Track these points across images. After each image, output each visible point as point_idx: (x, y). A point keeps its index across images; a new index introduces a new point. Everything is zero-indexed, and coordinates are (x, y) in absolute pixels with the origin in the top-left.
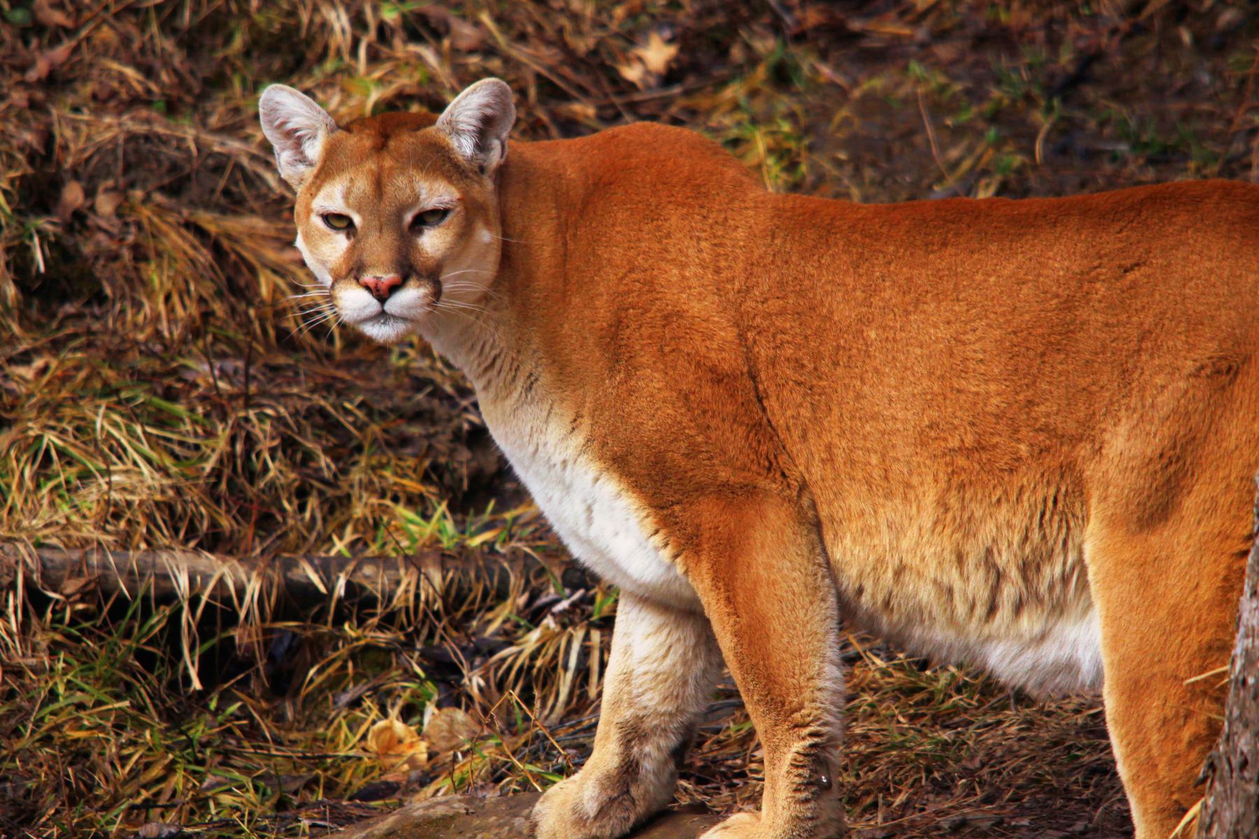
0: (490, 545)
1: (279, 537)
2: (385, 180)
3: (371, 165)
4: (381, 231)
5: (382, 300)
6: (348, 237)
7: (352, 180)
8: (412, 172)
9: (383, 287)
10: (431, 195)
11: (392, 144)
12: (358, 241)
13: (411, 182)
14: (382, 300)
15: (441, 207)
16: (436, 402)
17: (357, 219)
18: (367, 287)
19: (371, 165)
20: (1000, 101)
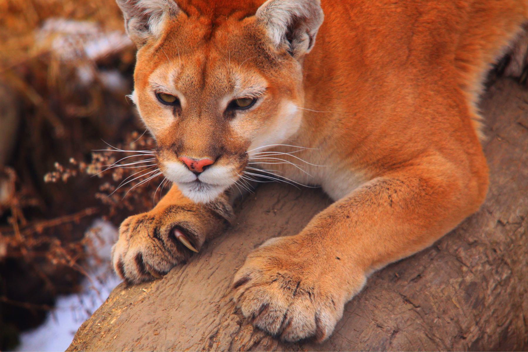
0: (501, 275)
1: (178, 54)
2: (209, 70)
3: (199, 55)
4: (200, 116)
5: (197, 174)
6: (174, 113)
7: (183, 67)
8: (230, 65)
9: (198, 166)
10: (245, 83)
11: (219, 33)
12: (183, 120)
13: (229, 73)
14: (197, 174)
15: (251, 96)
16: (230, 318)
17: (183, 101)
18: (184, 163)
19: (199, 55)
20: (472, 238)
